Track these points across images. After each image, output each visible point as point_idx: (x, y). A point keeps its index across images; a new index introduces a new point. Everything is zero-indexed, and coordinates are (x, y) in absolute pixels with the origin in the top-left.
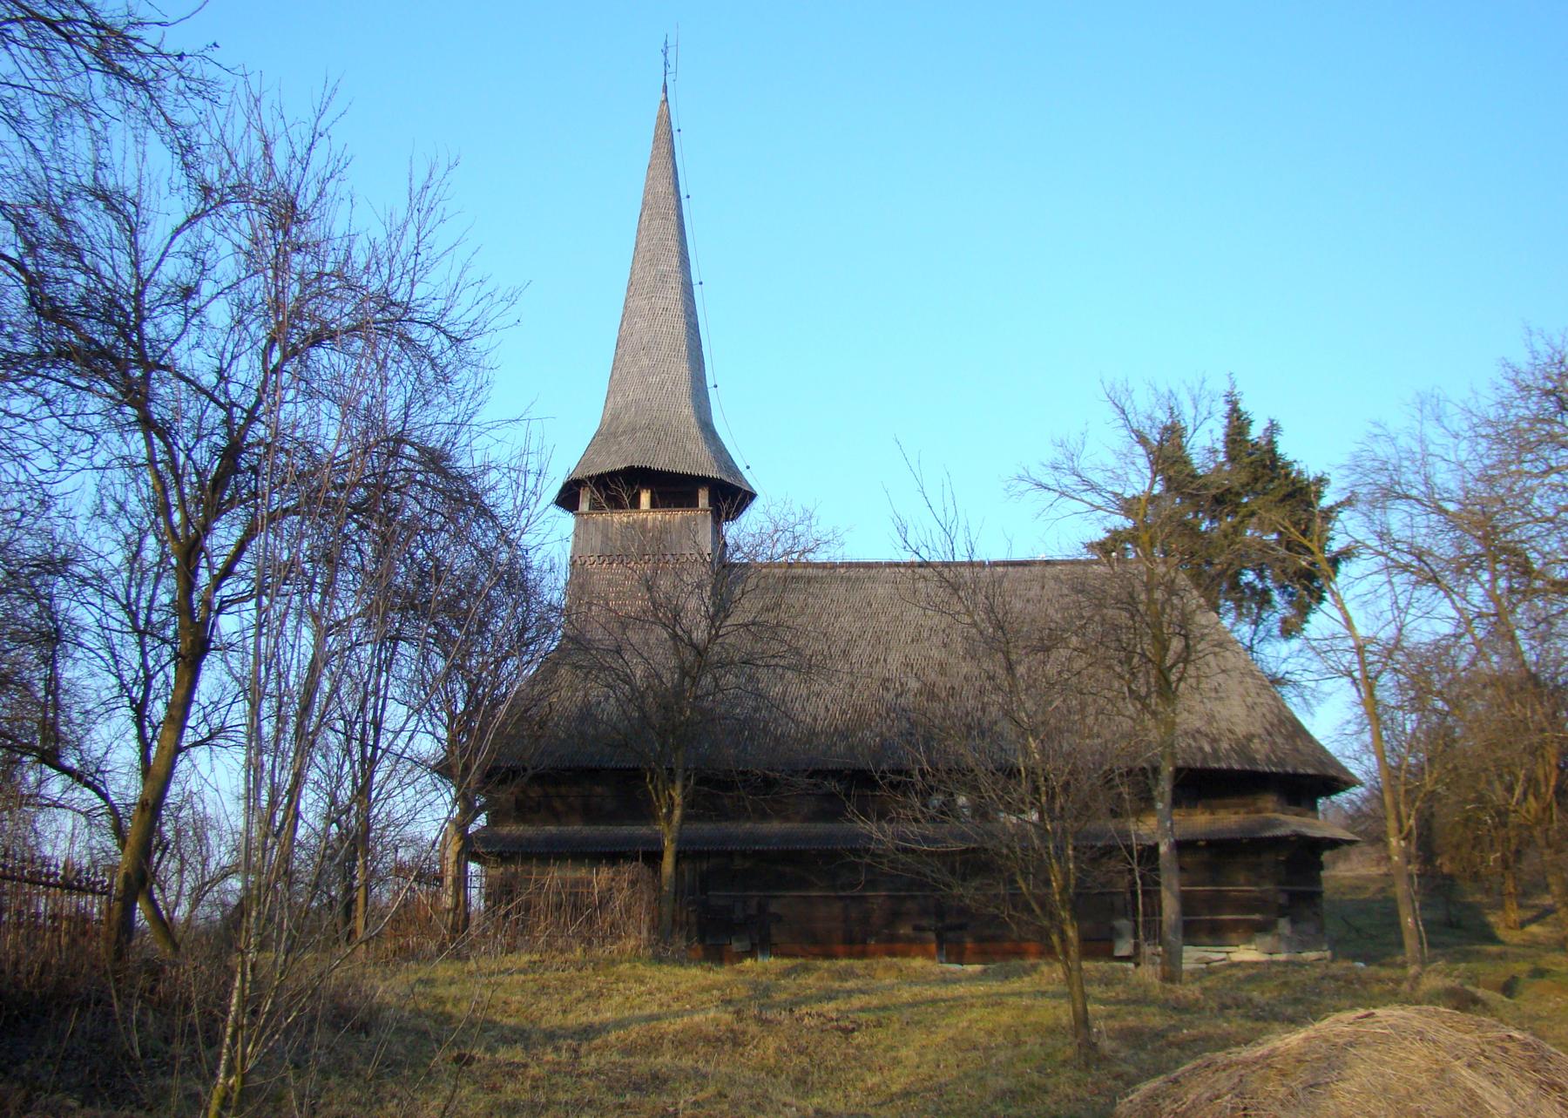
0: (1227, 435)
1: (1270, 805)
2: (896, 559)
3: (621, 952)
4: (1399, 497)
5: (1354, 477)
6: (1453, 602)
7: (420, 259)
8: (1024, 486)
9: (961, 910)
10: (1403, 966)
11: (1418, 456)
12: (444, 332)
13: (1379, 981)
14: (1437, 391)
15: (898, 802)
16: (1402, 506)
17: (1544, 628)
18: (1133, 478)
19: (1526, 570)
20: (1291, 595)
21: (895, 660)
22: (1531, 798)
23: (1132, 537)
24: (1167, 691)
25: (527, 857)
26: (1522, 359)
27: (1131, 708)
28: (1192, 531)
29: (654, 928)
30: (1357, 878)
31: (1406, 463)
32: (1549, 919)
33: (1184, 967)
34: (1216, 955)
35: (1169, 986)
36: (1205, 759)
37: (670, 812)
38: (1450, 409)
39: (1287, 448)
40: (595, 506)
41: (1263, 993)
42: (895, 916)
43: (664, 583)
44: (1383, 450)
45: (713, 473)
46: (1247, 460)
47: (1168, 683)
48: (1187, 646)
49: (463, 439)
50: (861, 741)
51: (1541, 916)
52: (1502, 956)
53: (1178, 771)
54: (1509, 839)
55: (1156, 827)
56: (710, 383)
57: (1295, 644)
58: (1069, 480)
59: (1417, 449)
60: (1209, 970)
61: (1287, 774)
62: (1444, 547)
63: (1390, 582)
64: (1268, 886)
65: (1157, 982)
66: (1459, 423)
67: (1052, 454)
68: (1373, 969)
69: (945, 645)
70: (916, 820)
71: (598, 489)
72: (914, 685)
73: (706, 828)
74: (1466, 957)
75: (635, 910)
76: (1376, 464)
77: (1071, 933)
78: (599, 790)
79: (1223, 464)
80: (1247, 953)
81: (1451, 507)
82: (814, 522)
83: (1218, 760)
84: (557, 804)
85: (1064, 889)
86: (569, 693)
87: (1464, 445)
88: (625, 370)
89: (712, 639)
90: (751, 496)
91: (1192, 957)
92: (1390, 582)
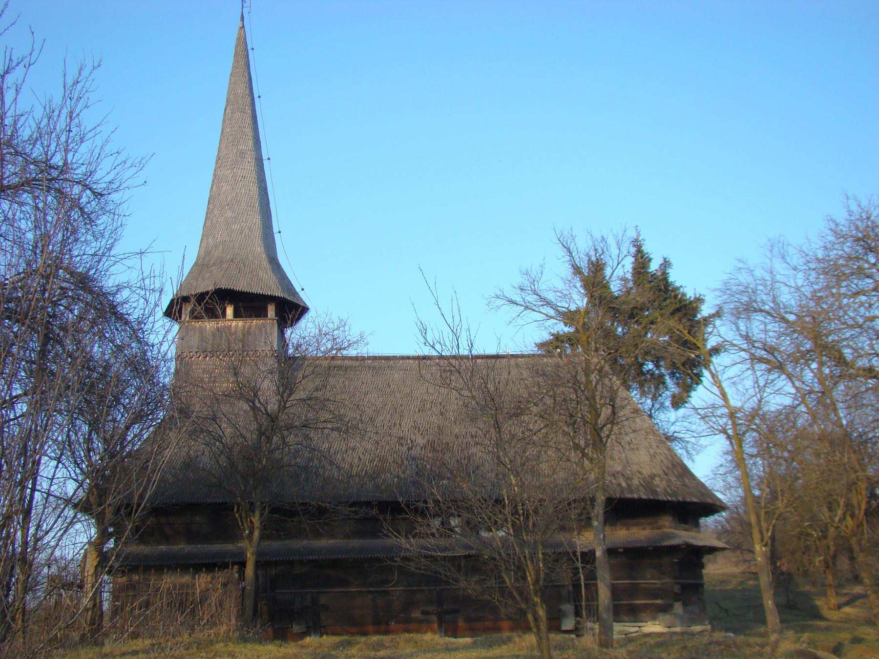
0: (634, 269)
1: (667, 524)
3: (217, 635)
4: (755, 311)
5: (725, 297)
6: (793, 383)
7: (71, 134)
8: (499, 302)
9: (456, 599)
10: (764, 635)
11: (769, 283)
12: (90, 189)
13: (749, 645)
14: (782, 239)
16: (759, 317)
17: (855, 401)
18: (576, 297)
19: (840, 360)
20: (677, 379)
21: (407, 423)
22: (848, 518)
23: (570, 339)
24: (599, 443)
25: (147, 569)
28: (608, 334)
29: (241, 615)
30: (723, 575)
31: (760, 287)
32: (858, 603)
33: (615, 637)
34: (631, 628)
35: (604, 650)
36: (622, 491)
37: (251, 533)
38: (791, 250)
39: (675, 277)
40: (195, 317)
41: (669, 654)
42: (409, 605)
43: (246, 371)
44: (744, 278)
45: (278, 293)
46: (649, 286)
47: (601, 439)
48: (614, 413)
49: (104, 265)
52: (828, 629)
53: (609, 501)
54: (828, 547)
55: (592, 539)
56: (275, 230)
57: (681, 411)
58: (531, 298)
60: (629, 639)
61: (679, 502)
62: (786, 345)
63: (753, 369)
64: (667, 580)
65: (596, 647)
66: (796, 260)
69: (442, 414)
70: (433, 535)
71: (199, 303)
72: (421, 441)
73: (275, 545)
74: (803, 629)
75: (227, 604)
76: (740, 288)
77: (541, 613)
78: (198, 518)
79: (631, 288)
80: (654, 627)
81: (792, 318)
82: (347, 328)
83: (632, 492)
84: (167, 530)
85: (537, 581)
86: (176, 449)
88: (215, 220)
91: (619, 629)
92: (753, 369)
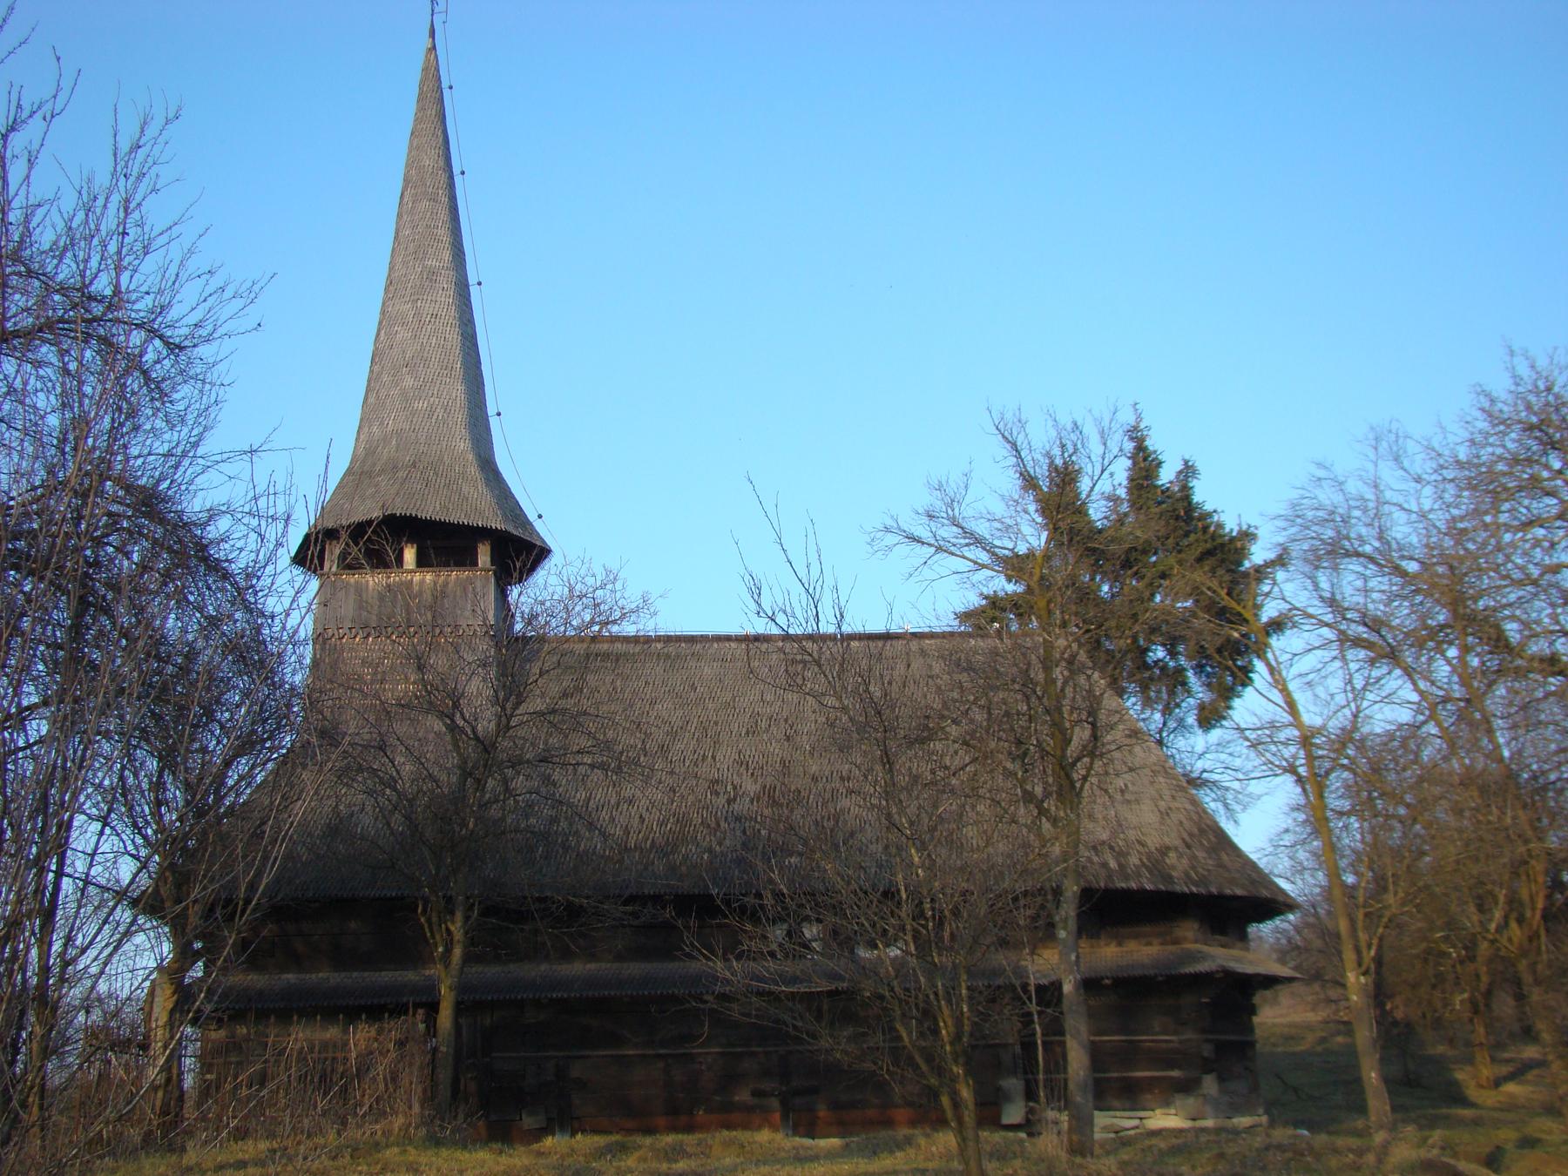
0: (1131, 480)
1: (1190, 935)
2: (751, 631)
4: (1347, 554)
5: (1293, 530)
6: (1414, 684)
7: (127, 240)
8: (891, 539)
9: (814, 1069)
11: (1371, 505)
12: (161, 337)
14: (1394, 426)
15: (745, 932)
16: (1354, 565)
17: (1525, 715)
18: (1027, 529)
19: (1499, 643)
20: (1208, 675)
21: (726, 756)
22: (1513, 925)
24: (1068, 791)
25: (262, 1015)
26: (1501, 386)
27: (1023, 813)
28: (1086, 596)
29: (429, 1098)
30: (1290, 1025)
31: (1356, 513)
33: (1097, 1136)
34: (1126, 1121)
35: (1078, 1160)
36: (1110, 877)
37: (449, 950)
38: (1411, 447)
39: (1205, 494)
40: (348, 565)
41: (1193, 1167)
43: (439, 661)
44: (1327, 496)
45: (496, 523)
48: (1095, 737)
49: (186, 471)
50: (686, 857)
51: (1520, 1072)
52: (1477, 1122)
53: (1087, 893)
54: (1478, 976)
55: (1055, 962)
56: (491, 411)
58: (948, 532)
59: (1370, 495)
60: (1122, 1141)
61: (1211, 896)
62: (1403, 615)
64: (1189, 1035)
65: (1063, 1155)
66: (1420, 463)
67: (927, 499)
68: (1322, 1139)
69: (788, 739)
71: (352, 541)
72: (751, 787)
73: (491, 972)
76: (1321, 513)
77: (966, 1093)
78: (353, 925)
79: (1126, 515)
80: (1166, 1119)
81: (1412, 567)
82: (618, 586)
83: (1127, 878)
85: (957, 1037)
86: (314, 801)
87: (1428, 491)
88: (383, 393)
89: (504, 727)
90: (543, 553)
91: (1105, 1122)
